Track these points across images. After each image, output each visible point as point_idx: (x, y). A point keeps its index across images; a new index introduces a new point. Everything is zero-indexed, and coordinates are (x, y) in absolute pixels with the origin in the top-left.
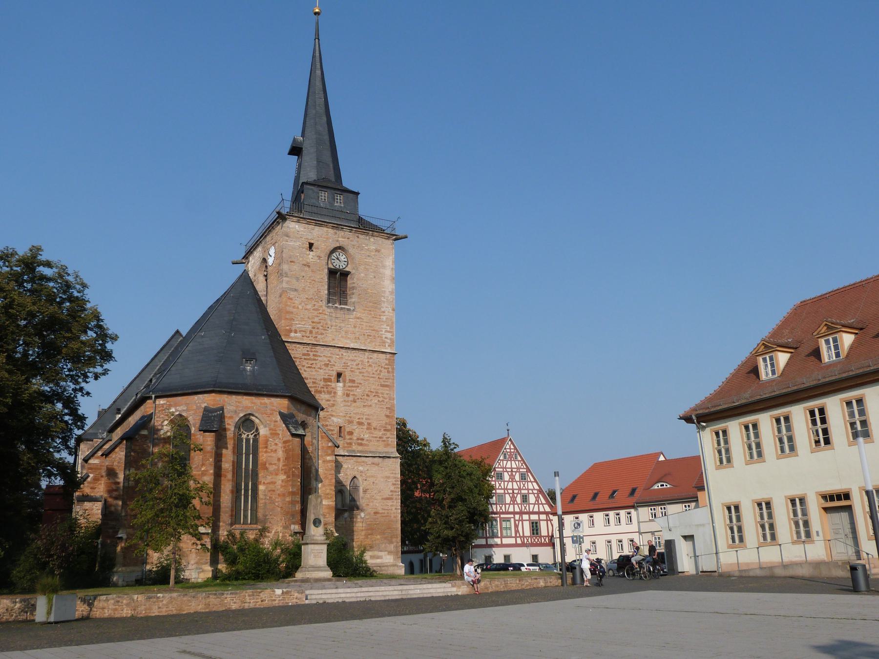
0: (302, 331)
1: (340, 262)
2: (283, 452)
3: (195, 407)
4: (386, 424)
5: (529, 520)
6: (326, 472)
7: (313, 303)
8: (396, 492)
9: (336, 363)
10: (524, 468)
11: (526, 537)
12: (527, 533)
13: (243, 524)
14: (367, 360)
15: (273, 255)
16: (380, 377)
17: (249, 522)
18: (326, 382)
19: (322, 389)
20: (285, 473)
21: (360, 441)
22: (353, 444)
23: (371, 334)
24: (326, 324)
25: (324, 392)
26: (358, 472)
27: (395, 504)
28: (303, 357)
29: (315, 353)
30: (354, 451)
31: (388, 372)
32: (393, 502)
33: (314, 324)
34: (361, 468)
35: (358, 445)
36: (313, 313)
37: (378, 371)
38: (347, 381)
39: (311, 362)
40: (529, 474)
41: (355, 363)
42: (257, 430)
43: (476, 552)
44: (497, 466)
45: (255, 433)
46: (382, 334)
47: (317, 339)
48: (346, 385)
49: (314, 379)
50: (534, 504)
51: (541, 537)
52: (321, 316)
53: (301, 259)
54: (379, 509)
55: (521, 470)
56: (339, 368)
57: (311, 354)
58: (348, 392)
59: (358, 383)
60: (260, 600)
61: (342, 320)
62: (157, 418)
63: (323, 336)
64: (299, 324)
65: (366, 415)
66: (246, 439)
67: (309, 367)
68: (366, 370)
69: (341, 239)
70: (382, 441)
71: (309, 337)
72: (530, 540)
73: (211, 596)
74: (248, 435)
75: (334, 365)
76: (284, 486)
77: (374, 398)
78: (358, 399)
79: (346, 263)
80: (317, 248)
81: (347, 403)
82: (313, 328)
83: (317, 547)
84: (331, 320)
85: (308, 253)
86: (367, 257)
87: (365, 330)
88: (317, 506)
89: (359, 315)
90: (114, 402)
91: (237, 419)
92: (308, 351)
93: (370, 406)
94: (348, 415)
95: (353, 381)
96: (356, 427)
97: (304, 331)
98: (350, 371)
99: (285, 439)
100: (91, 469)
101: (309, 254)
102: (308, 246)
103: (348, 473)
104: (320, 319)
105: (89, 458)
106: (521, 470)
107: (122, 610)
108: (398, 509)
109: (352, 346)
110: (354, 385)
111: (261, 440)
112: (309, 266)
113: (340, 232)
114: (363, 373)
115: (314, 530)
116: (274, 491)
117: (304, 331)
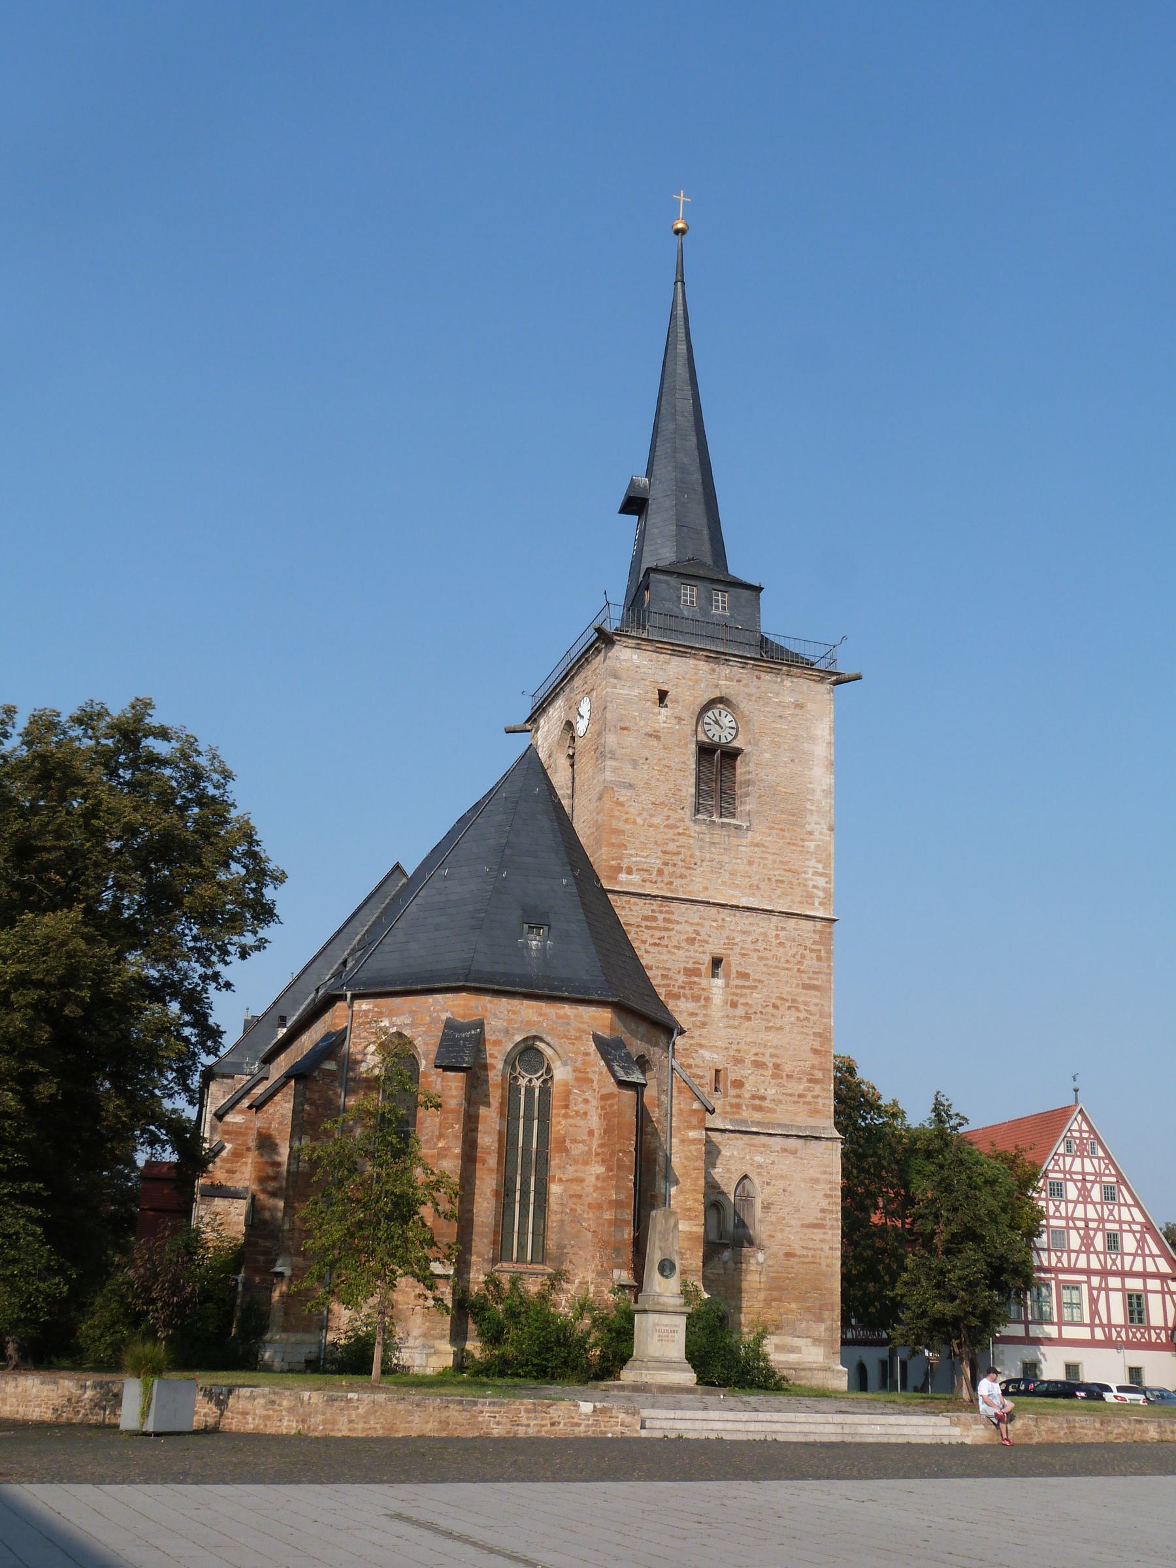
0: (643, 870)
1: (721, 729)
2: (600, 1118)
3: (428, 1018)
4: (813, 1067)
5: (1123, 1289)
6: (686, 1163)
8: (831, 1212)
10: (1111, 1175)
11: (1116, 1326)
12: (1118, 1317)
14: (774, 933)
15: (587, 715)
16: (802, 968)
17: (529, 1258)
19: (682, 991)
21: (757, 1102)
22: (744, 1108)
23: (784, 878)
24: (692, 856)
25: (685, 996)
28: (644, 923)
29: (667, 916)
30: (745, 1122)
31: (819, 959)
32: (824, 1233)
33: (667, 857)
34: (759, 1159)
37: (798, 957)
39: (658, 934)
40: (1122, 1187)
42: (549, 1070)
43: (1002, 1352)
45: (545, 1077)
46: (806, 880)
51: (1149, 1328)
52: (682, 840)
53: (642, 723)
55: (1104, 1179)
56: (716, 947)
57: (661, 917)
58: (735, 998)
59: (755, 980)
60: (548, 1422)
62: (355, 1037)
63: (684, 881)
67: (655, 944)
69: (724, 682)
71: (656, 882)
73: (451, 1406)
74: (530, 1081)
75: (707, 942)
77: (788, 1012)
78: (755, 1013)
79: (733, 732)
81: (731, 1022)
82: (666, 864)
83: (666, 1319)
84: (701, 848)
87: (770, 869)
89: (758, 838)
92: (653, 911)
93: (780, 1028)
95: (745, 976)
96: (750, 1072)
97: (646, 870)
98: (740, 954)
99: (604, 1091)
103: (733, 1169)
105: (226, 1113)
106: (1104, 1179)
108: (836, 1249)
109: (744, 902)
110: (747, 984)
111: (556, 1090)
112: (658, 738)
113: (722, 667)
116: (580, 1197)
117: (646, 870)
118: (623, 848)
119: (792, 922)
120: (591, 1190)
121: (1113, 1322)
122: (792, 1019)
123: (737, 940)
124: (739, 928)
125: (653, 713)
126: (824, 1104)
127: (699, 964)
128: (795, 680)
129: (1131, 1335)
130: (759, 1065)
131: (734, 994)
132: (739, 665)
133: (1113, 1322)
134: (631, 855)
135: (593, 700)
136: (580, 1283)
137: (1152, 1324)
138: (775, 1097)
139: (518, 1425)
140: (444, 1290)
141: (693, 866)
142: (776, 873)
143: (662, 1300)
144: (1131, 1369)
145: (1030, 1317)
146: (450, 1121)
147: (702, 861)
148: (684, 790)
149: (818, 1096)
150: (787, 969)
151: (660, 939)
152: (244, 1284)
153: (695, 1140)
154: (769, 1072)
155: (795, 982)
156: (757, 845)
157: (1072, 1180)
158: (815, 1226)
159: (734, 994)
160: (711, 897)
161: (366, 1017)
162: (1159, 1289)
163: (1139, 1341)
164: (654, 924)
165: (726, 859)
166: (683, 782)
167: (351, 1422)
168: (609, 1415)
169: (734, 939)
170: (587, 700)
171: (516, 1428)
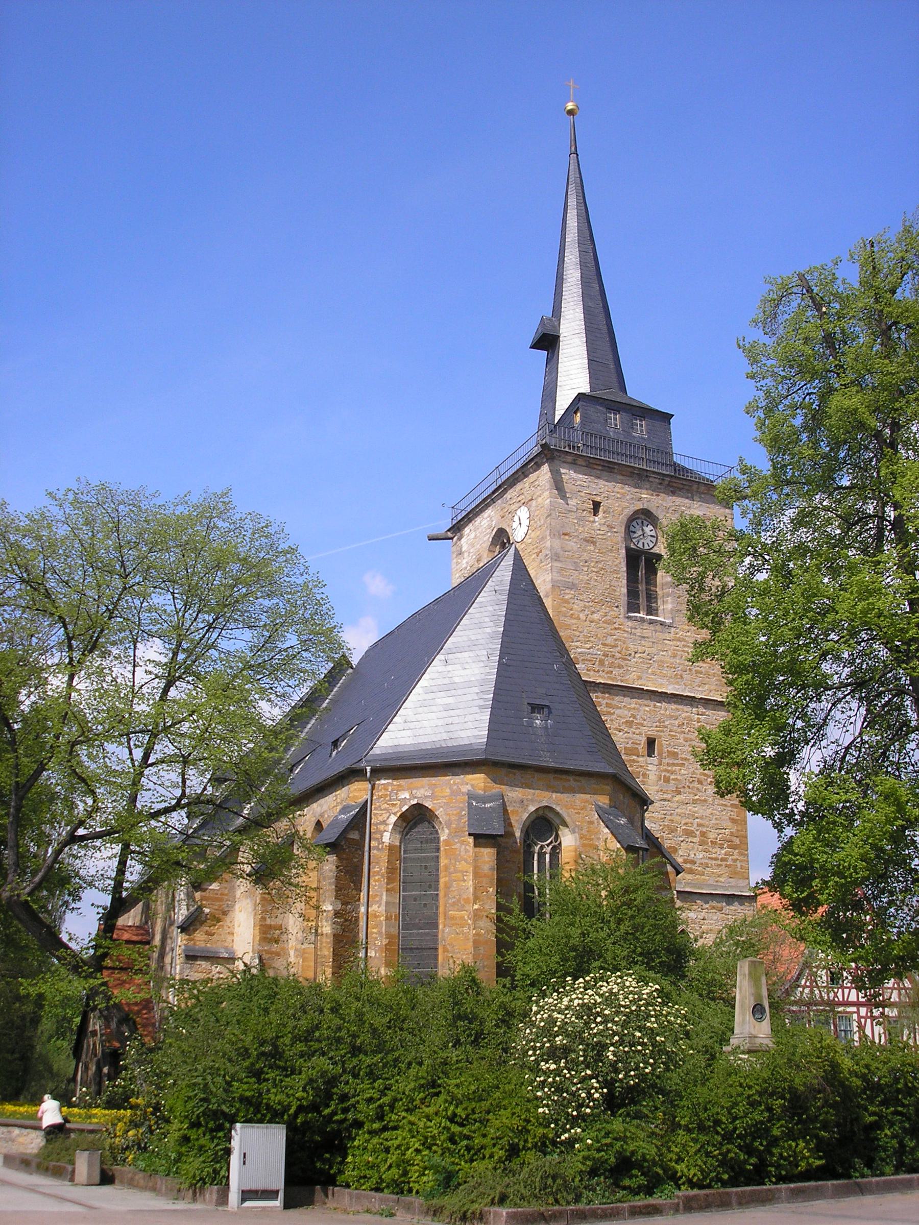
0: (587, 660)
3: (448, 790)
4: (732, 834)
7: (604, 609)
15: (525, 522)
24: (627, 649)
48: (664, 761)
58: (668, 775)
59: (682, 759)
62: (376, 809)
63: (621, 671)
70: (726, 866)
71: (598, 671)
75: (642, 725)
79: (654, 540)
85: (591, 519)
91: (525, 815)
93: (705, 801)
94: (668, 817)
95: (674, 755)
96: (682, 839)
101: (594, 522)
104: (616, 640)
110: (676, 762)
112: (594, 543)
114: (691, 740)
124: (668, 713)
131: (666, 771)
132: (657, 480)
135: (532, 509)
138: (703, 861)
159: (666, 771)
161: (386, 790)
166: (616, 584)
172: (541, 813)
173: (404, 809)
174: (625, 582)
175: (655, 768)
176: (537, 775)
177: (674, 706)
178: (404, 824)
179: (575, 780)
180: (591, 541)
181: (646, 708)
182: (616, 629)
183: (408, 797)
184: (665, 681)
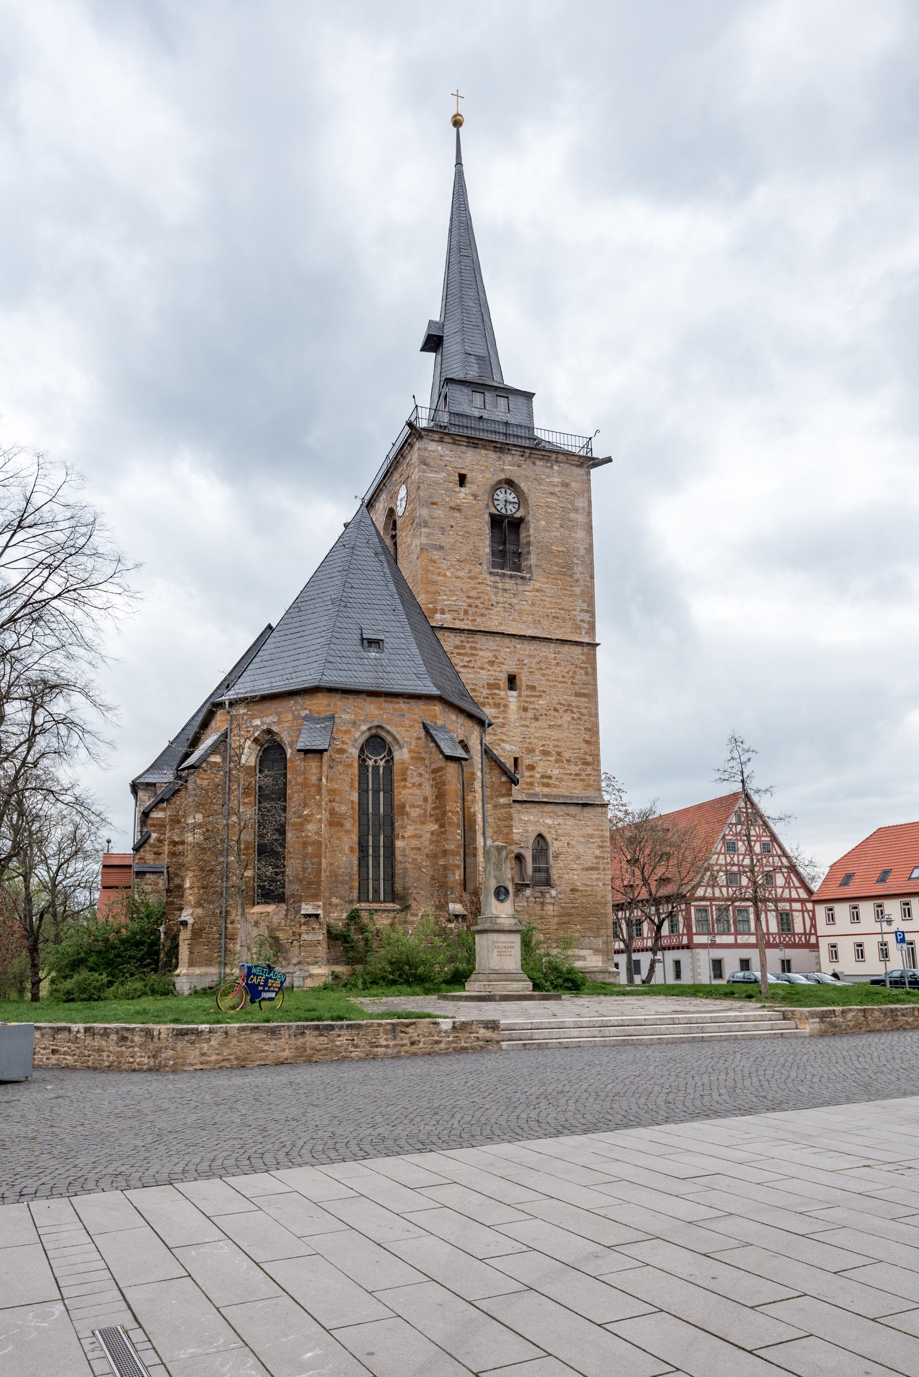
0: (453, 611)
1: (506, 502)
2: (432, 787)
3: (291, 716)
4: (585, 753)
5: (776, 910)
6: (499, 823)
7: (468, 567)
8: (603, 858)
9: (505, 659)
10: (766, 836)
11: (772, 934)
12: (774, 927)
13: (373, 901)
14: (553, 656)
16: (575, 681)
17: (382, 898)
18: (491, 689)
19: (486, 700)
20: (436, 820)
21: (545, 780)
22: (536, 785)
23: (558, 615)
24: (489, 600)
25: (489, 704)
26: (544, 826)
27: (601, 877)
28: (456, 651)
29: (473, 645)
30: (536, 795)
31: (587, 674)
32: (599, 874)
33: (471, 601)
34: (549, 821)
35: (543, 786)
36: (469, 583)
37: (571, 673)
38: (524, 688)
39: (467, 659)
40: (775, 844)
41: (534, 661)
42: (390, 752)
43: (698, 954)
44: (727, 833)
45: (387, 758)
46: (575, 616)
47: (476, 623)
49: (473, 684)
50: (784, 888)
51: (794, 934)
52: (482, 588)
53: (447, 499)
54: (579, 884)
55: (763, 839)
56: (510, 667)
57: (468, 646)
58: (526, 705)
60: (406, 1041)
61: (514, 594)
62: (234, 736)
63: (484, 619)
64: (448, 600)
65: (554, 740)
66: (373, 767)
67: (464, 666)
68: (552, 671)
69: (508, 467)
70: (581, 780)
71: (463, 620)
72: (777, 940)
73: (307, 1032)
74: (376, 761)
75: (503, 664)
76: (434, 842)
77: (564, 714)
78: (541, 715)
80: (472, 483)
81: (524, 723)
82: (470, 606)
83: (503, 938)
84: (496, 593)
86: (550, 496)
87: (548, 609)
88: (501, 865)
89: (538, 585)
90: (183, 730)
92: (462, 642)
93: (560, 726)
94: (528, 741)
95: (533, 688)
96: (539, 758)
97: (455, 611)
98: (528, 672)
99: (434, 766)
100: (154, 825)
101: (460, 492)
102: (458, 479)
103: (530, 829)
105: (151, 810)
106: (763, 839)
107: (132, 1057)
108: (608, 885)
109: (529, 633)
111: (396, 768)
112: (459, 510)
113: (506, 455)
115: (496, 908)
116: (419, 849)
117: (455, 611)
118: (437, 594)
119: (566, 649)
120: (427, 843)
121: (771, 931)
122: (569, 719)
123: (526, 661)
124: (527, 653)
125: (454, 491)
126: (594, 780)
127: (498, 680)
128: (561, 465)
129: (792, 939)
130: (545, 753)
132: (518, 453)
133: (771, 931)
134: (444, 600)
136: (422, 916)
137: (796, 932)
138: (559, 776)
139: (377, 1047)
140: (314, 926)
141: (490, 607)
142: (553, 611)
143: (499, 921)
144: (783, 961)
145: (716, 932)
146: (312, 793)
147: (498, 603)
148: (481, 549)
149: (589, 775)
150: (564, 682)
151: (468, 662)
152: (165, 933)
153: (505, 804)
154: (553, 759)
155: (570, 691)
156: (538, 591)
157: (741, 840)
158: (591, 869)
160: (505, 630)
162: (800, 909)
163: (788, 943)
164: (463, 651)
165: (514, 601)
167: (203, 1054)
168: (469, 1031)
169: (523, 661)
170: (404, 487)
171: (376, 1049)
172: (374, 731)
173: (256, 734)
174: (488, 542)
175: (515, 699)
176: (369, 699)
177: (535, 646)
178: (259, 748)
179: (404, 703)
180: (457, 509)
181: (505, 649)
182: (479, 583)
183: (259, 724)
184: (524, 626)
